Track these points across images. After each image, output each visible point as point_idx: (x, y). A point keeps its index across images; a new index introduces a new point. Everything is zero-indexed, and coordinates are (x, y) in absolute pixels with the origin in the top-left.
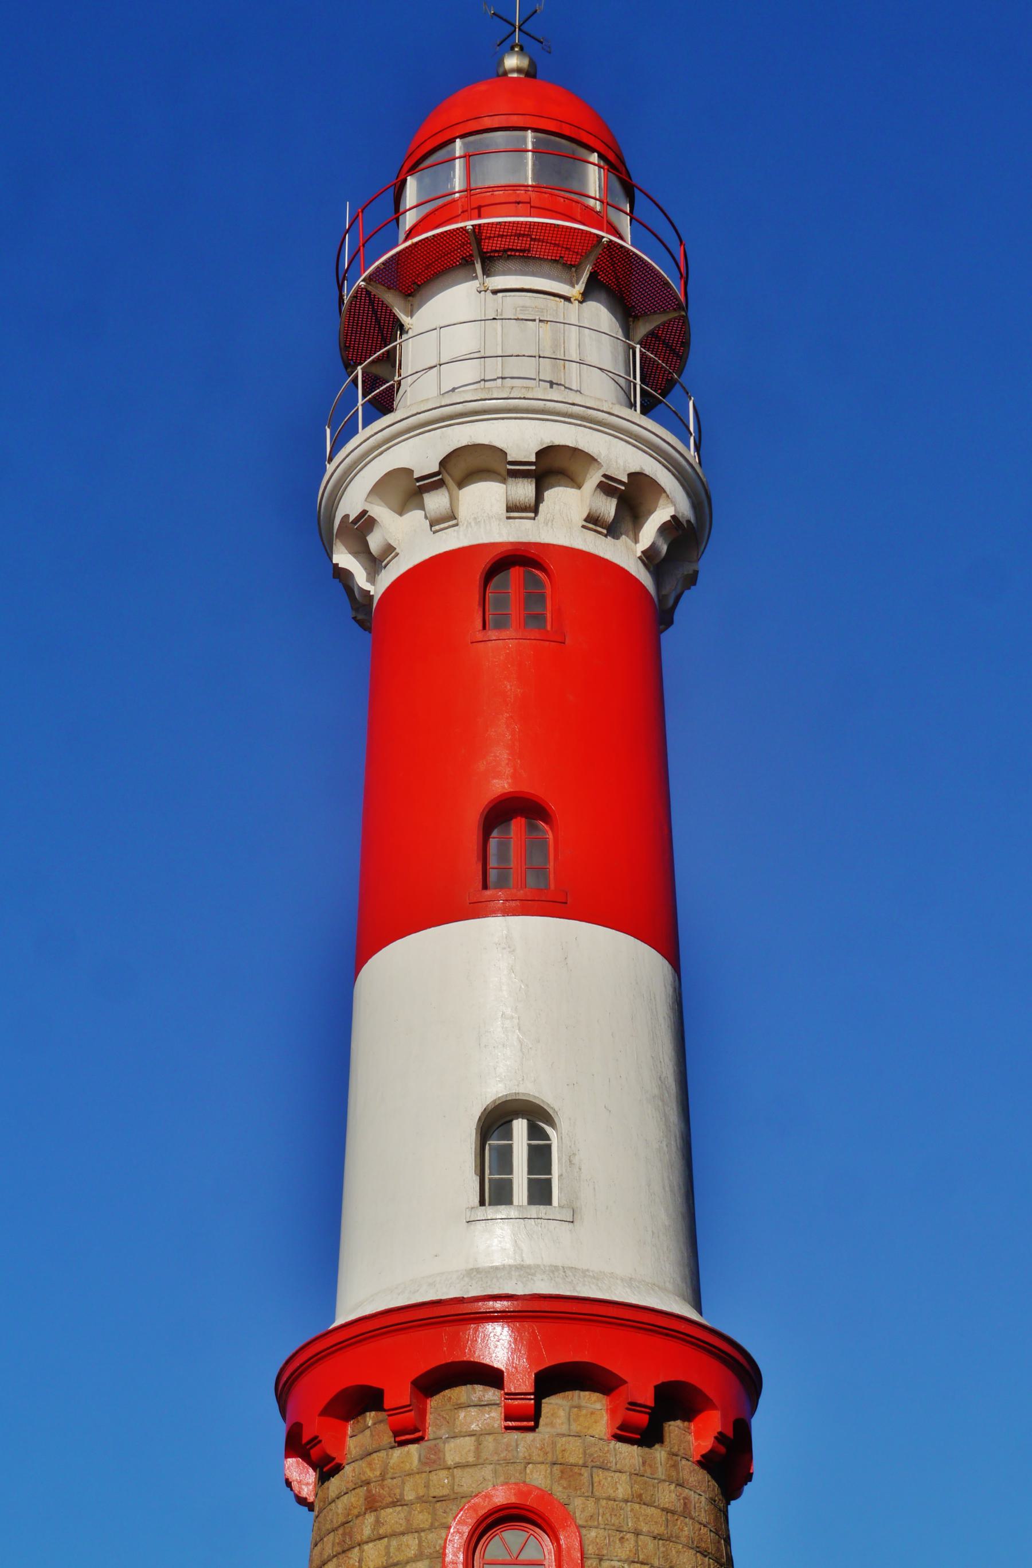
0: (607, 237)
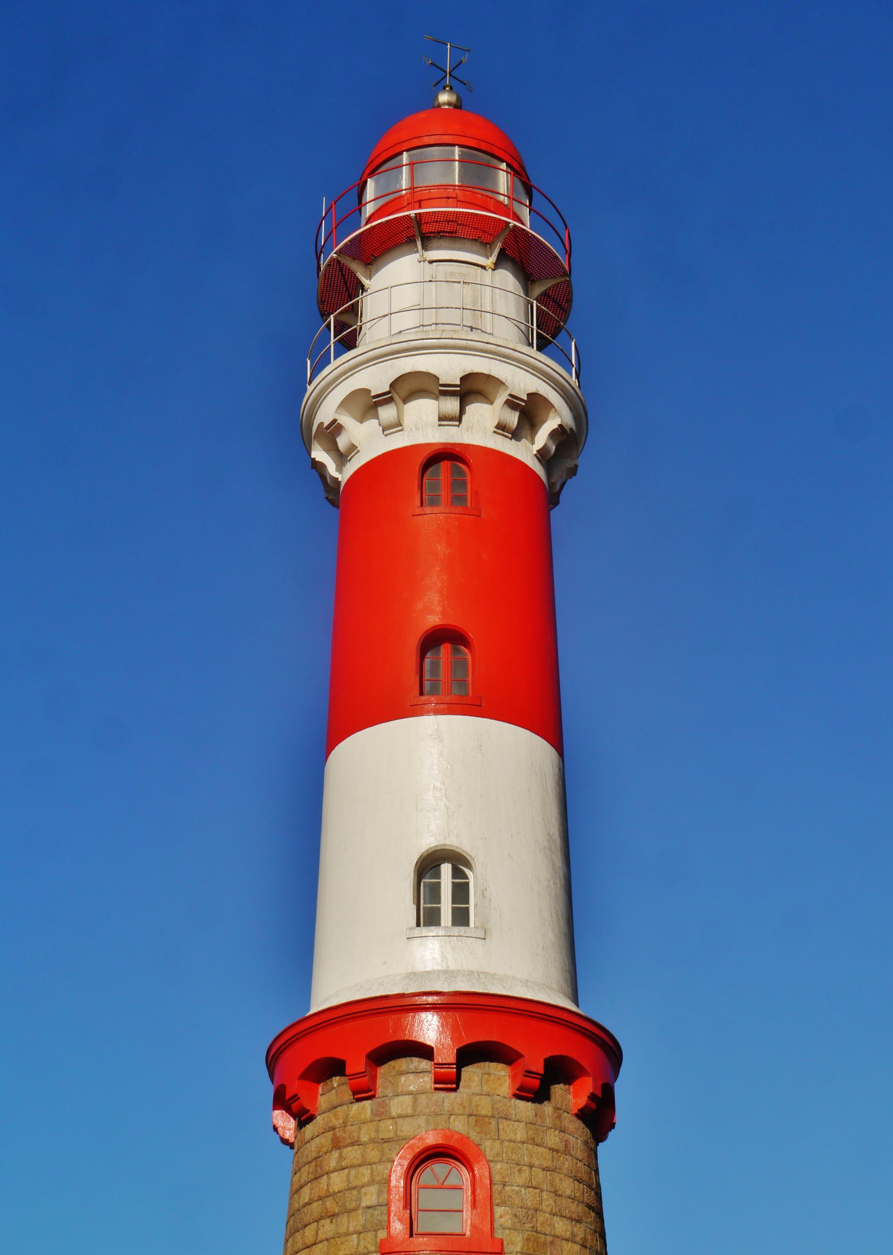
0: (513, 223)
